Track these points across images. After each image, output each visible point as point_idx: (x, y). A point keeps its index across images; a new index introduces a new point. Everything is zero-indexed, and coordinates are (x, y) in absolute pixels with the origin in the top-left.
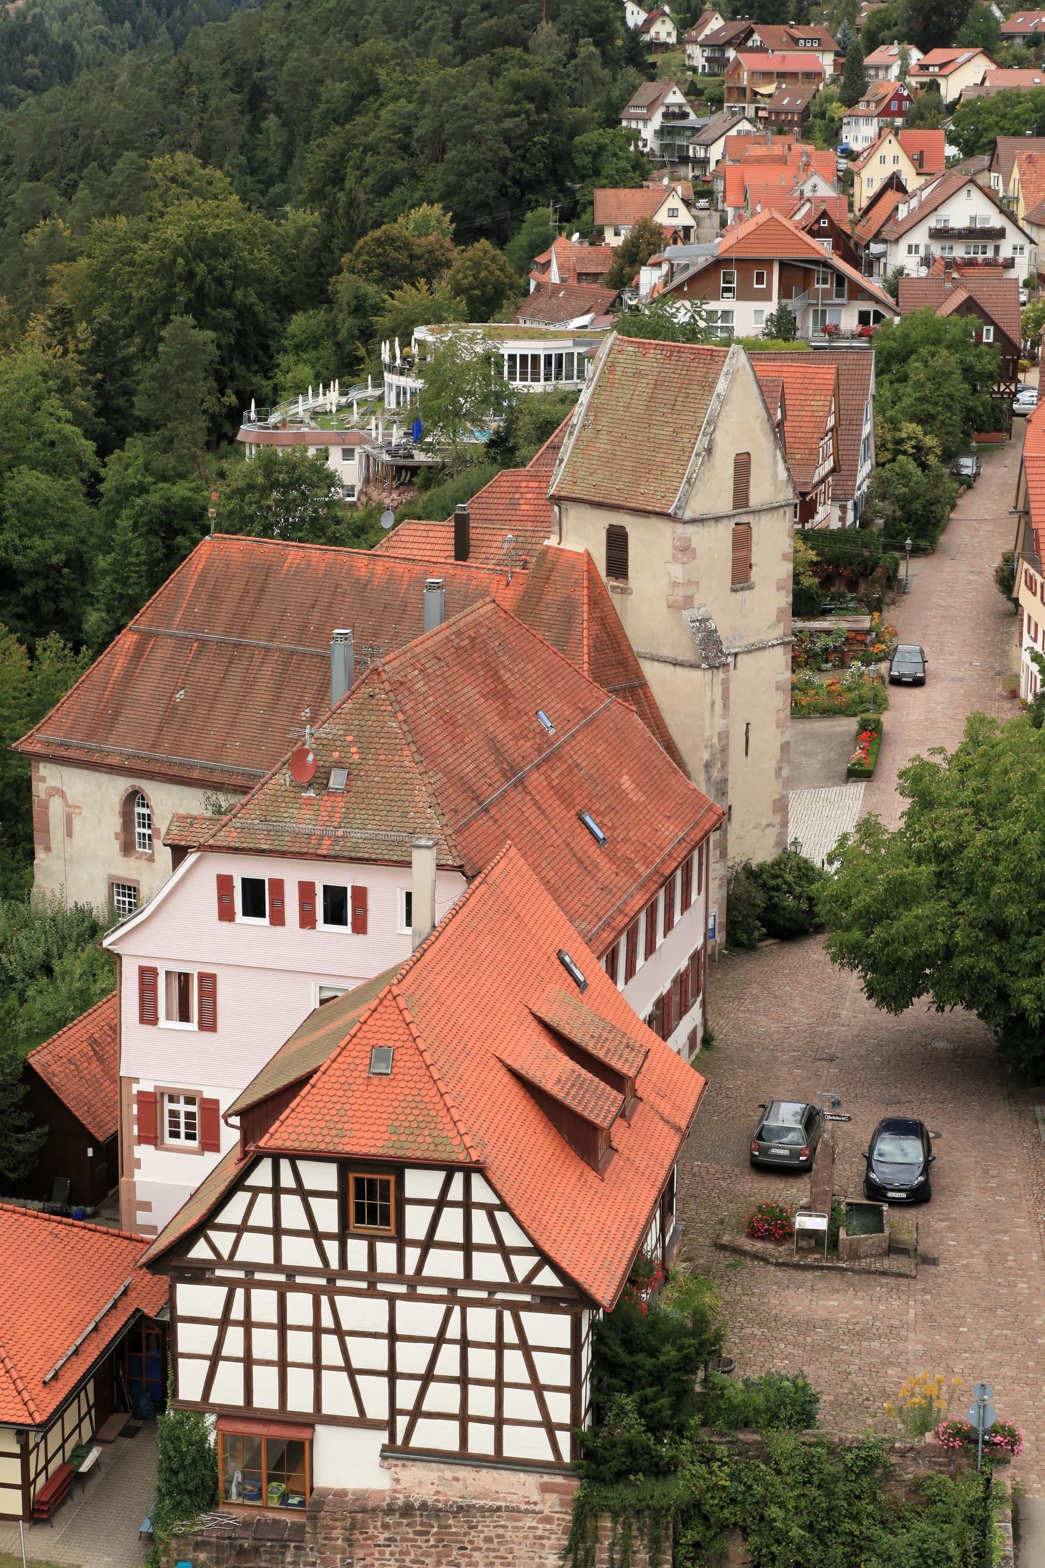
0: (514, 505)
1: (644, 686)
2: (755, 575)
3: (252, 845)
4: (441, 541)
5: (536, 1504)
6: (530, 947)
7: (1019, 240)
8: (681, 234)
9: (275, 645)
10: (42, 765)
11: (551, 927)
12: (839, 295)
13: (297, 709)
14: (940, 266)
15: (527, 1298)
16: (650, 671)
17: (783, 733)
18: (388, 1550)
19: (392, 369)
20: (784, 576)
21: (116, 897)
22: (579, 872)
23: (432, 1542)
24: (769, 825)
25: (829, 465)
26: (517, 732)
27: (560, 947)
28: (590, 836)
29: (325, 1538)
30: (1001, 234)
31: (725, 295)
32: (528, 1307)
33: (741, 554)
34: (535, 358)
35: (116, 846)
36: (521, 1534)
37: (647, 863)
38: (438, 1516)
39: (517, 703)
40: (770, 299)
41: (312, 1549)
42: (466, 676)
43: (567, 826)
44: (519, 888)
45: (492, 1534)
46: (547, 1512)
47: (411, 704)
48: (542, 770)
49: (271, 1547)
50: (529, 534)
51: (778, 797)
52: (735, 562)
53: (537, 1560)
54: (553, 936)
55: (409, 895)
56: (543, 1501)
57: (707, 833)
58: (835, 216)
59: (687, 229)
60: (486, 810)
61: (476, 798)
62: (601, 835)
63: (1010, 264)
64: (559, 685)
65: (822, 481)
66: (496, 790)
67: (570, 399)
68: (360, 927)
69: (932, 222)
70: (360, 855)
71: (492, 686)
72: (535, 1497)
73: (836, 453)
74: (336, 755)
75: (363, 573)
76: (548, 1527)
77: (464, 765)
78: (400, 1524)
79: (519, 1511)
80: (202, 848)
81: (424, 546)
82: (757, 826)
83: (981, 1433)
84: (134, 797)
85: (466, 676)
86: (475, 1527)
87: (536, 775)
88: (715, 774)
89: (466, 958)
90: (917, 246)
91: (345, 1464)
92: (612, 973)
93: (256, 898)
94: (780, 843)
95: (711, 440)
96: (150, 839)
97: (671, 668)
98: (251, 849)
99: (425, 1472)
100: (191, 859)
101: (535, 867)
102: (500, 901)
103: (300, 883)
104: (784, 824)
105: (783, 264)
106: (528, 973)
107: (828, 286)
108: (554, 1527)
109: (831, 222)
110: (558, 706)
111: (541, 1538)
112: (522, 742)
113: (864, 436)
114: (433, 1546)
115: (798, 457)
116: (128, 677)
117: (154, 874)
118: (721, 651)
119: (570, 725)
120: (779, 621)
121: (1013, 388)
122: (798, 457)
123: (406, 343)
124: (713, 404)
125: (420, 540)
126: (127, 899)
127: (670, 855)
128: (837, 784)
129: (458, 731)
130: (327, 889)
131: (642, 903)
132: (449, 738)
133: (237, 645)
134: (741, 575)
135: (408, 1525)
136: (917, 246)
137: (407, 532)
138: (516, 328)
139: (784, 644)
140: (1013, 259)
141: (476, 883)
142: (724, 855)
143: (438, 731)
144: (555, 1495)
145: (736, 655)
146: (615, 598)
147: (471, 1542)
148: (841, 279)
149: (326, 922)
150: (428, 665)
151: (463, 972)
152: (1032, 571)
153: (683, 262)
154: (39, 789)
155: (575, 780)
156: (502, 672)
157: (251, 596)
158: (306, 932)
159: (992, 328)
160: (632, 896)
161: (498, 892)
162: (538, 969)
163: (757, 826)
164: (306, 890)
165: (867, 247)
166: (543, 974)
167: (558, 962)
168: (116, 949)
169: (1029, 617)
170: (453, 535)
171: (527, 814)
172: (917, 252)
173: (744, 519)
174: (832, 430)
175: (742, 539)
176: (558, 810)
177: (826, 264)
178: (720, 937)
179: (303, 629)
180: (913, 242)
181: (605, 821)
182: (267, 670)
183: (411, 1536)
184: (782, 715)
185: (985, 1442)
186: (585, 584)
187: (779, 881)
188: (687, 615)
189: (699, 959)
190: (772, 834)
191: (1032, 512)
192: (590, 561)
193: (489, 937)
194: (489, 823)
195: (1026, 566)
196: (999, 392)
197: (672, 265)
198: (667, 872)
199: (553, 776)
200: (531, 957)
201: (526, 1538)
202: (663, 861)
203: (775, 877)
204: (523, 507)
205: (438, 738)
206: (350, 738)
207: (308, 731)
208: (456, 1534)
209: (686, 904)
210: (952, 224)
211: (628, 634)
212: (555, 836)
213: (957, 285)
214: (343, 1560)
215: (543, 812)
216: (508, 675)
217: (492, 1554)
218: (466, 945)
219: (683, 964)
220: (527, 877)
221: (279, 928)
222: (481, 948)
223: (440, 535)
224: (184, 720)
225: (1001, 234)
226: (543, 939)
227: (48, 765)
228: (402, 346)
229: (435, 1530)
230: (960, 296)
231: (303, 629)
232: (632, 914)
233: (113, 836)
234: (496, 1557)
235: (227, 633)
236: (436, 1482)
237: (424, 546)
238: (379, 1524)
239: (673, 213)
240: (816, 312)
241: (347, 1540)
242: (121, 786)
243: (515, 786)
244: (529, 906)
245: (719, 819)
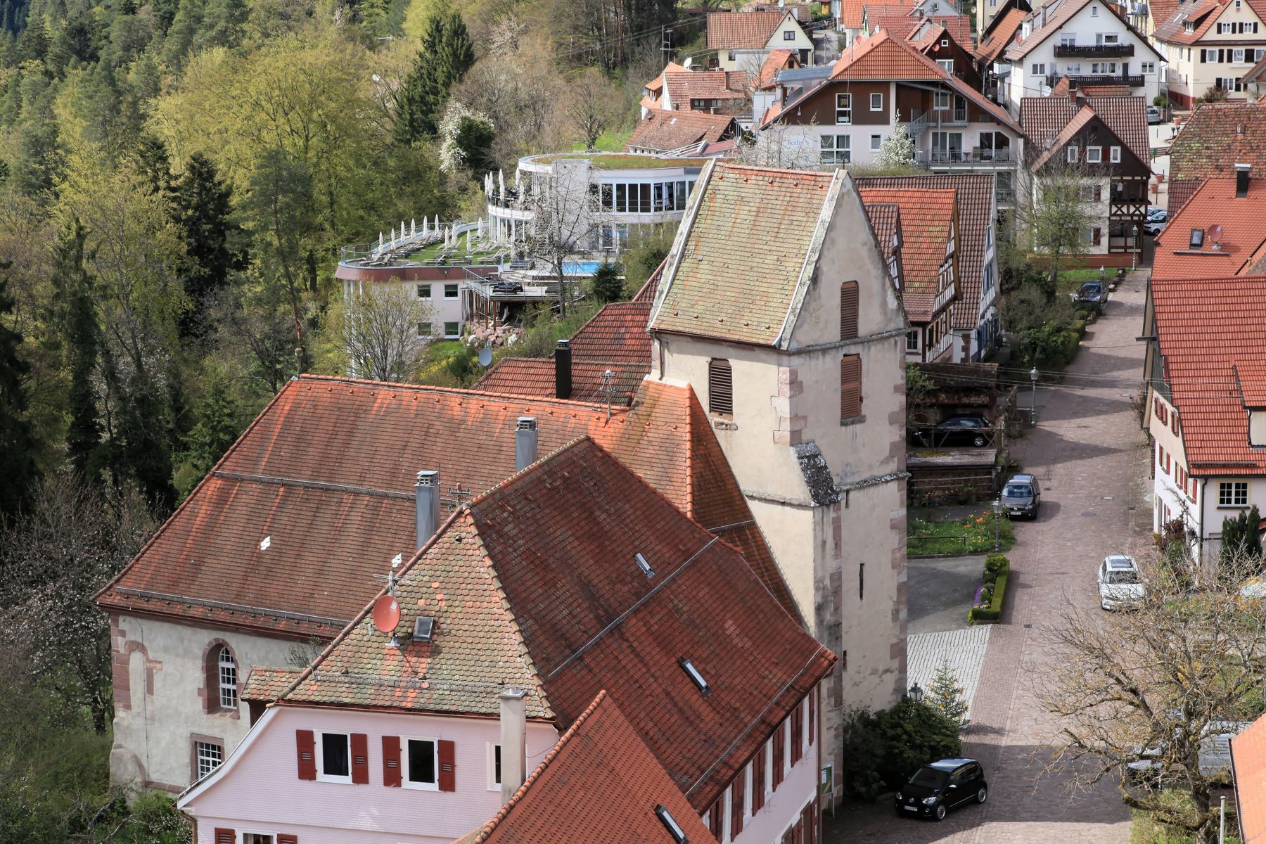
0: (619, 339)
1: (753, 526)
2: (866, 409)
3: (333, 699)
4: (541, 378)
6: (626, 802)
7: (1149, 58)
8: (799, 57)
9: (365, 488)
10: (121, 619)
11: (648, 782)
12: (960, 117)
13: (389, 556)
14: (1064, 85)
16: (753, 506)
17: (899, 573)
19: (496, 202)
20: (897, 409)
21: (200, 757)
22: (680, 722)
24: (886, 671)
25: (951, 291)
26: (614, 575)
27: (659, 802)
28: (691, 685)
30: (1129, 51)
31: (841, 119)
33: (852, 386)
34: (645, 188)
35: (199, 704)
37: (754, 712)
39: (614, 546)
40: (887, 122)
42: (559, 518)
43: (667, 675)
44: (614, 740)
47: (499, 548)
48: (640, 615)
50: (633, 369)
51: (895, 641)
52: (845, 395)
54: (651, 790)
55: (498, 749)
57: (818, 678)
58: (957, 37)
59: (804, 52)
60: (581, 659)
61: (569, 646)
62: (703, 683)
63: (1140, 82)
64: (659, 526)
65: (943, 309)
66: (591, 637)
67: (673, 227)
68: (448, 784)
69: (1057, 40)
70: (446, 707)
71: (587, 528)
73: (958, 280)
74: (421, 602)
75: (457, 411)
77: (556, 612)
80: (284, 702)
81: (524, 384)
82: (874, 672)
84: (217, 652)
85: (559, 518)
87: (634, 621)
88: (828, 617)
89: (556, 814)
90: (1042, 66)
92: (717, 830)
93: (339, 755)
94: (900, 688)
95: (816, 269)
96: (235, 695)
97: (780, 507)
98: (332, 704)
100: (268, 715)
101: (631, 718)
102: (594, 754)
103: (384, 738)
104: (903, 669)
105: (900, 86)
106: (624, 830)
107: (948, 108)
109: (952, 42)
110: (658, 548)
112: (618, 586)
113: (986, 262)
115: (917, 285)
116: (211, 527)
117: (236, 733)
118: (832, 489)
119: (670, 568)
120: (892, 456)
121: (1143, 210)
122: (917, 285)
123: (509, 175)
125: (520, 377)
126: (211, 759)
127: (777, 704)
128: (959, 627)
129: (550, 576)
130: (327, 738)
131: (747, 754)
132: (540, 584)
133: (326, 489)
134: (851, 409)
136: (1042, 66)
137: (506, 370)
138: (625, 157)
139: (898, 479)
140: (1143, 77)
141: (568, 734)
142: (839, 702)
143: (529, 576)
145: (848, 492)
146: (720, 435)
148: (960, 100)
149: (411, 779)
150: (518, 507)
151: (553, 830)
152: (1162, 400)
153: (797, 86)
154: (119, 643)
155: (676, 625)
156: (597, 513)
157: (339, 440)
158: (391, 791)
159: (1119, 149)
160: (738, 748)
161: (591, 745)
162: (634, 826)
163: (874, 672)
164: (390, 745)
165: (991, 67)
166: (639, 831)
167: (655, 818)
168: (192, 811)
169: (1161, 448)
170: (554, 372)
171: (624, 663)
172: (1042, 71)
173: (853, 350)
174: (952, 256)
175: (851, 371)
176: (657, 657)
177: (944, 86)
178: (837, 791)
179: (394, 471)
180: (1038, 61)
181: (708, 669)
182: (356, 517)
184: (898, 555)
186: (688, 421)
187: (899, 730)
189: (812, 813)
190: (890, 679)
191: (1162, 338)
192: (693, 397)
193: (582, 793)
194: (583, 672)
195: (1156, 394)
196: (1128, 215)
197: (785, 90)
198: (776, 721)
199: (652, 622)
200: (627, 813)
202: (770, 711)
203: (894, 726)
204: (629, 342)
205: (529, 584)
206: (436, 585)
207: (390, 577)
209: (797, 755)
210: (1078, 43)
211: (735, 471)
212: (655, 685)
213: (1081, 103)
215: (642, 661)
216: (604, 516)
218: (556, 802)
219: (795, 819)
220: (623, 728)
221: (449, 794)
222: (573, 804)
223: (540, 372)
224: (270, 569)
225: (1129, 51)
226: (640, 794)
227: (128, 619)
228: (506, 178)
230: (1085, 116)
231: (394, 471)
232: (737, 766)
233: (196, 691)
235: (316, 477)
237: (524, 384)
239: (789, 36)
240: (935, 135)
242: (203, 639)
243: (611, 632)
244: (625, 758)
245: (831, 664)
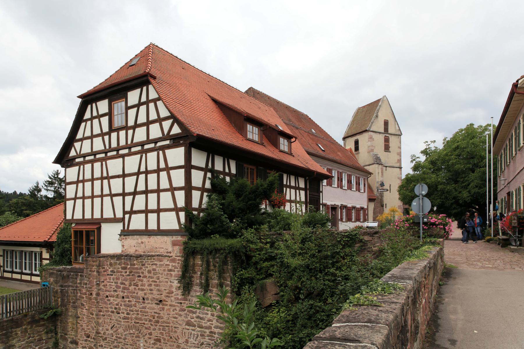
2: (390, 149)
5: (170, 253)
15: (168, 142)
18: (112, 277)
23: (128, 273)
29: (90, 271)
32: (168, 147)
36: (162, 269)
38: (130, 259)
41: (86, 276)
45: (151, 269)
46: (174, 257)
49: (73, 275)
53: (169, 283)
56: (173, 250)
72: (170, 249)
76: (174, 264)
78: (116, 263)
79: (162, 256)
83: (421, 216)
86: (144, 265)
91: (111, 241)
99: (132, 241)
108: (176, 264)
111: (170, 270)
114: (129, 275)
124: (378, 107)
135: (119, 264)
144: (178, 247)
146: (356, 156)
147: (143, 273)
173: (387, 135)
183: (120, 269)
185: (425, 223)
188: (372, 153)
201: (164, 270)
208: (137, 268)
214: (96, 282)
217: (151, 280)
229: (129, 266)
234: (152, 281)
236: (136, 245)
238: (109, 263)
241: (98, 272)
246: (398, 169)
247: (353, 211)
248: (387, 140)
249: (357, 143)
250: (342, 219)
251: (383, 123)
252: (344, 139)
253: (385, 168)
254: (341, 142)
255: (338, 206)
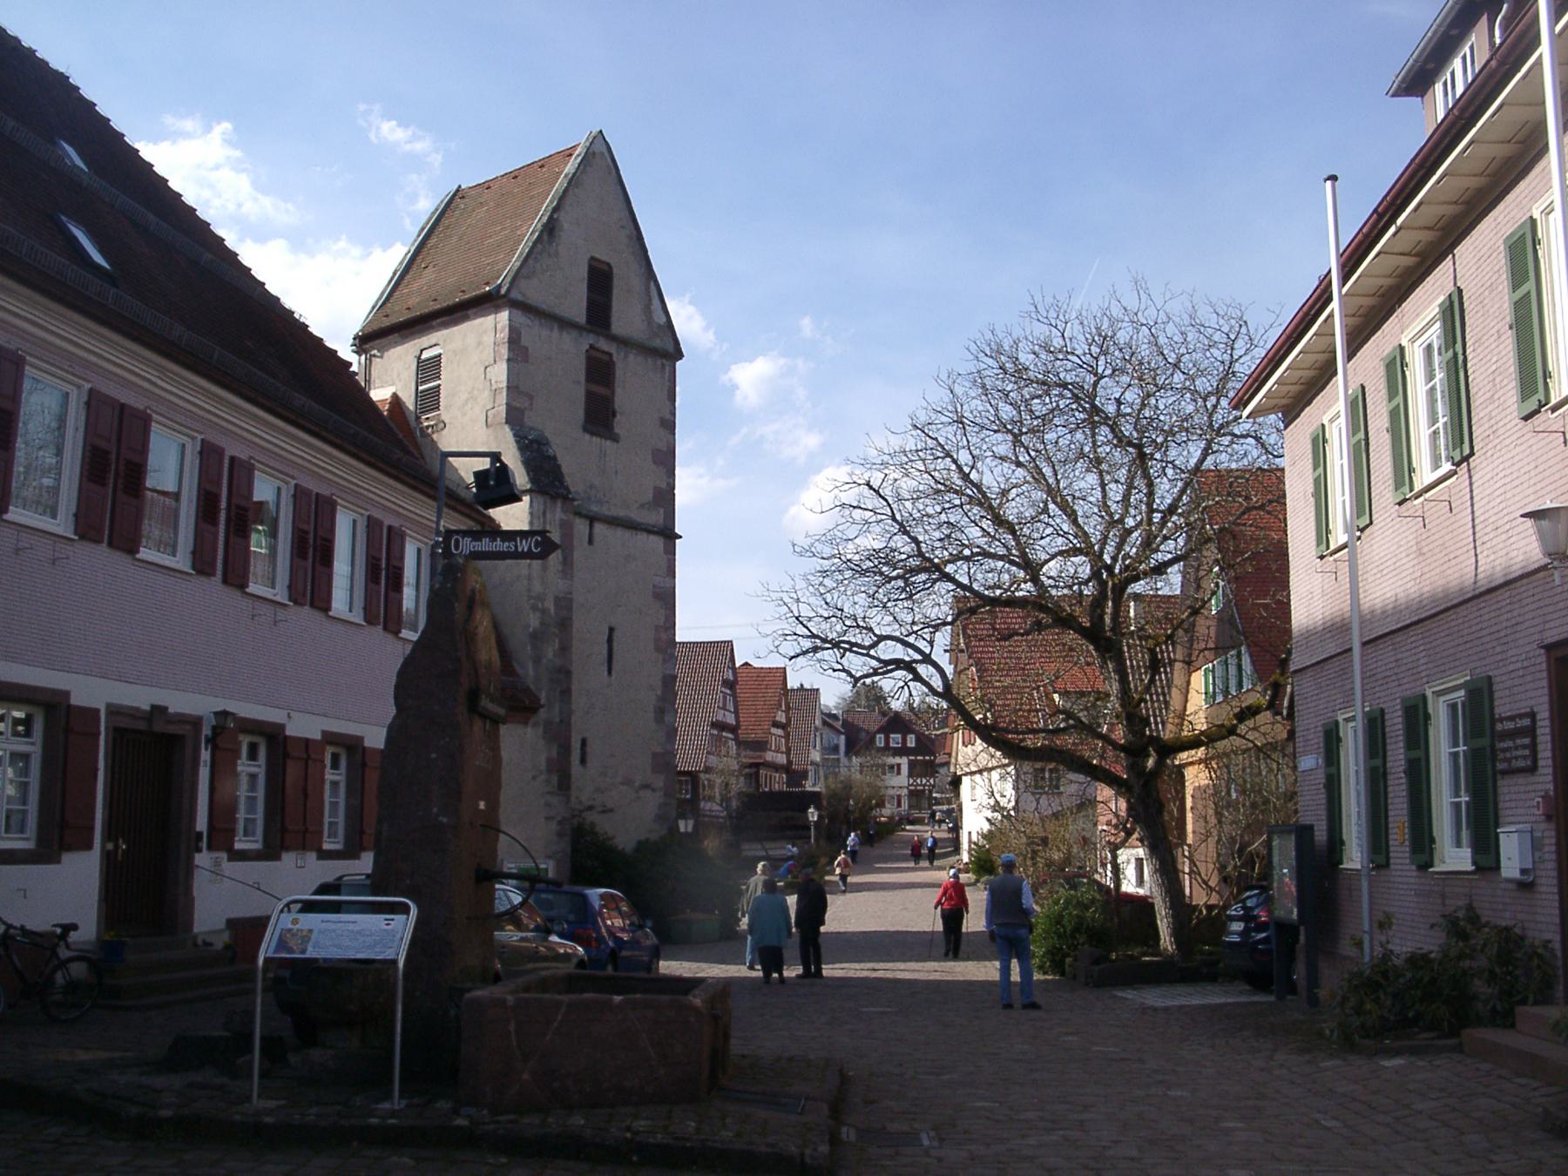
2: (620, 424)
173: (603, 345)
246: (657, 542)
247: (334, 776)
248: (600, 371)
249: (429, 369)
250: (221, 836)
251: (584, 272)
252: (364, 342)
253: (581, 526)
254: (346, 352)
255: (196, 722)
